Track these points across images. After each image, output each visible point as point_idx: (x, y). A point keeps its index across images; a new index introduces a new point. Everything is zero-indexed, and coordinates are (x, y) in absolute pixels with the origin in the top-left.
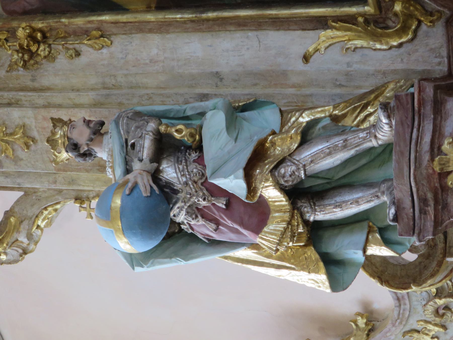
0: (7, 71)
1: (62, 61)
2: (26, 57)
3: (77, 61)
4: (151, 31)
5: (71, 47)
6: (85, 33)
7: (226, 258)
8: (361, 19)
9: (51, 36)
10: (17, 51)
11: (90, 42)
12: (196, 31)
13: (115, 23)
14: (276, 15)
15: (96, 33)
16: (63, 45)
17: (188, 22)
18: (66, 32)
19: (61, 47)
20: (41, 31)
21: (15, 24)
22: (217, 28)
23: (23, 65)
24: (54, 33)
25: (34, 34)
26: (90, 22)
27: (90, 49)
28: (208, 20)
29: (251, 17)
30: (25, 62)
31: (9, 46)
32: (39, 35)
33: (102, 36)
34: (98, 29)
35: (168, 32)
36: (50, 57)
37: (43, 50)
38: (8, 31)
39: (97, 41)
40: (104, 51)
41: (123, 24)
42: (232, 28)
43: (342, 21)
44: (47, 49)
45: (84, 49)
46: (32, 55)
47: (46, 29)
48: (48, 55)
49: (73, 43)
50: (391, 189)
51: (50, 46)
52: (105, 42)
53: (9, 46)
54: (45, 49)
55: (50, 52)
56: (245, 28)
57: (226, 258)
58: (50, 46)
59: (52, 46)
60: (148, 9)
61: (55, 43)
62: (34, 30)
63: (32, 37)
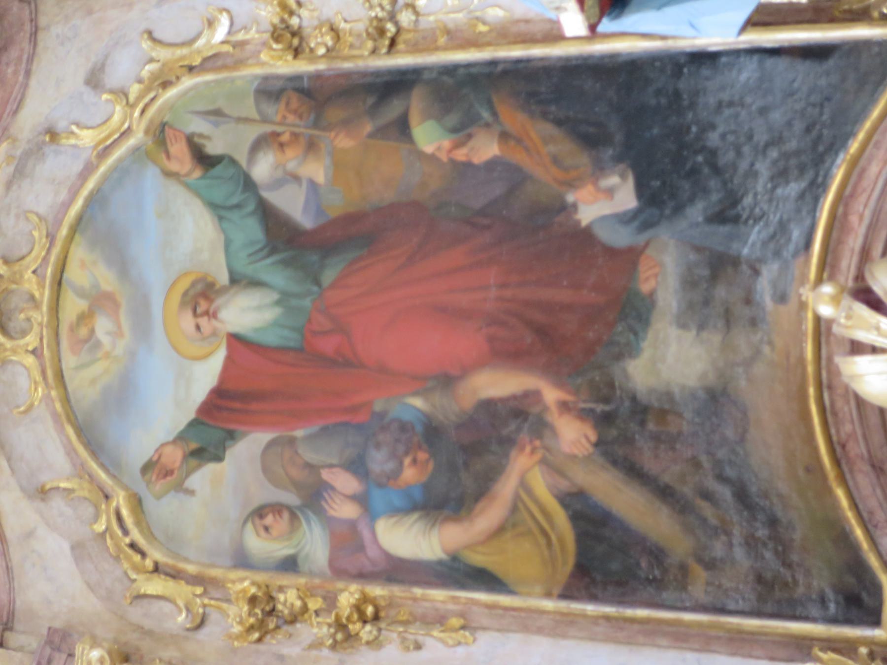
0: (304, 650)
1: (392, 651)
2: (339, 636)
3: (415, 655)
4: (540, 631)
5: (411, 637)
6: (439, 620)
7: (663, 38)
8: (863, 650)
9: (387, 617)
10: (330, 625)
11: (442, 635)
12: (608, 639)
13: (491, 607)
14: (738, 624)
15: (455, 622)
16: (400, 632)
17: (601, 621)
18: (411, 614)
19: (395, 635)
20: (373, 601)
21: (340, 585)
22: (641, 639)
23: (331, 645)
24: (393, 612)
25: (363, 607)
26: (454, 598)
27: (440, 645)
28: (632, 621)
29: (699, 624)
30: (335, 642)
31: (318, 623)
32: (370, 610)
33: (463, 628)
34: (462, 615)
35: (564, 636)
36: (375, 644)
37: (367, 632)
38: (325, 598)
39: (454, 635)
40: (460, 650)
41: (500, 612)
42: (664, 642)
43: (835, 650)
44: (375, 632)
45: (429, 642)
46: (350, 637)
47: (382, 603)
48: (374, 640)
49: (415, 632)
50: (814, 133)
51: (380, 630)
52: (465, 637)
53: (318, 623)
54: (371, 632)
55: (376, 638)
56: (684, 645)
57: (663, 38)
58: (380, 630)
59: (383, 632)
60: (548, 595)
61: (389, 628)
62: (365, 599)
63: (358, 608)
